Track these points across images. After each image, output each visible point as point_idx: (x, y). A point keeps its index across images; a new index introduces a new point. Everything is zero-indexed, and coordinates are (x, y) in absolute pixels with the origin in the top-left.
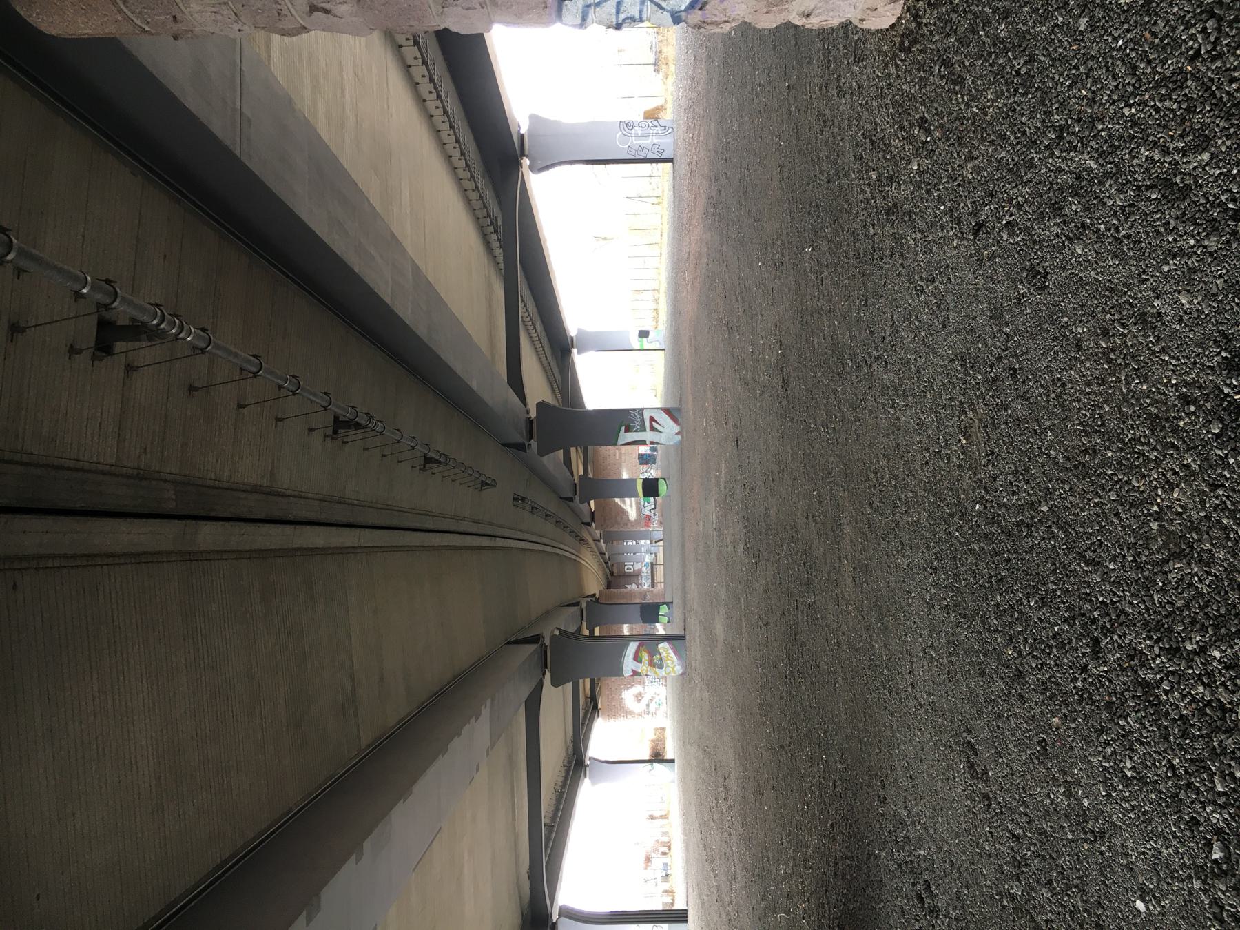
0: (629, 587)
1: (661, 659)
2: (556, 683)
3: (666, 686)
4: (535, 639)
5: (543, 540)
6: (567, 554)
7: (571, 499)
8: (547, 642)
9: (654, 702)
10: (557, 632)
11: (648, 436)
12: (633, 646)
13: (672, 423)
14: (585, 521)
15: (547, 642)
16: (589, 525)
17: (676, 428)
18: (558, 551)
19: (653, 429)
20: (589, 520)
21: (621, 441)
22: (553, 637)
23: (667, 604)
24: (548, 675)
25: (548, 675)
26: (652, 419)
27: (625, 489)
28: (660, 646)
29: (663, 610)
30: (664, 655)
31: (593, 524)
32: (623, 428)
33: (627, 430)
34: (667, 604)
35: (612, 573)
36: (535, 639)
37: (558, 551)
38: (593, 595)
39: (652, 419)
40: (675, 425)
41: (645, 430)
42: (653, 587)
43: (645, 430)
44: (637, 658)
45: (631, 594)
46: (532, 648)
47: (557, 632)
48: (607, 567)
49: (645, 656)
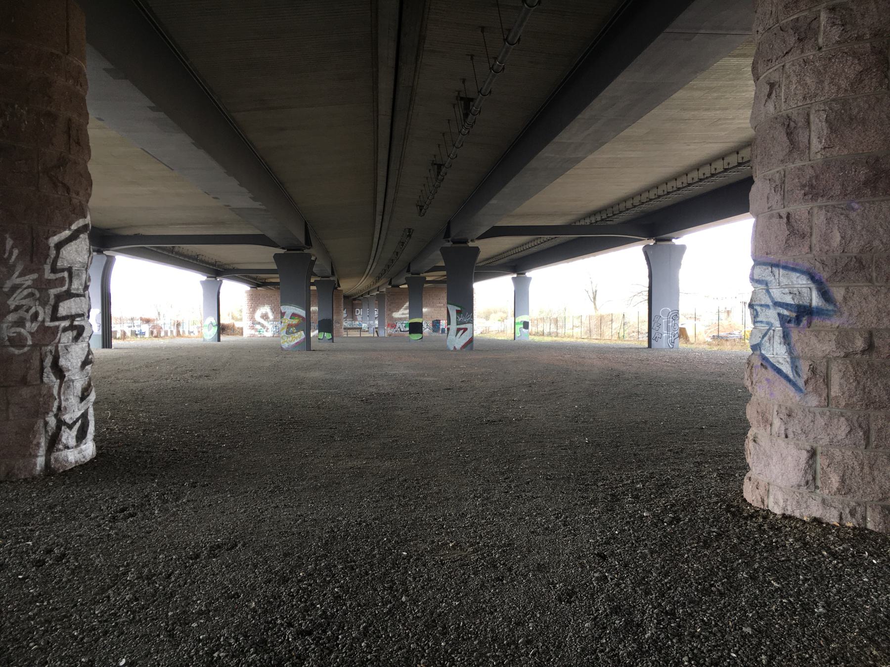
0: (345, 312)
1: (293, 333)
2: (276, 257)
3: (273, 336)
4: (308, 243)
5: (380, 250)
6: (369, 267)
7: (408, 271)
8: (306, 251)
9: (261, 328)
10: (313, 258)
11: (454, 327)
12: (302, 313)
13: (462, 344)
14: (392, 281)
15: (306, 251)
16: (390, 284)
17: (458, 347)
18: (371, 261)
19: (458, 330)
20: (393, 283)
21: (450, 307)
22: (310, 255)
23: (332, 339)
24: (282, 251)
25: (282, 251)
26: (465, 330)
27: (415, 310)
28: (302, 332)
29: (328, 336)
30: (296, 335)
31: (390, 287)
32: (459, 309)
33: (458, 312)
34: (332, 339)
35: (355, 299)
36: (308, 243)
37: (371, 261)
38: (339, 286)
39: (465, 330)
40: (460, 346)
41: (457, 325)
42: (345, 329)
43: (457, 325)
44: (294, 315)
45: (339, 313)
46: (302, 239)
47: (313, 258)
48: (359, 297)
49: (295, 321)
